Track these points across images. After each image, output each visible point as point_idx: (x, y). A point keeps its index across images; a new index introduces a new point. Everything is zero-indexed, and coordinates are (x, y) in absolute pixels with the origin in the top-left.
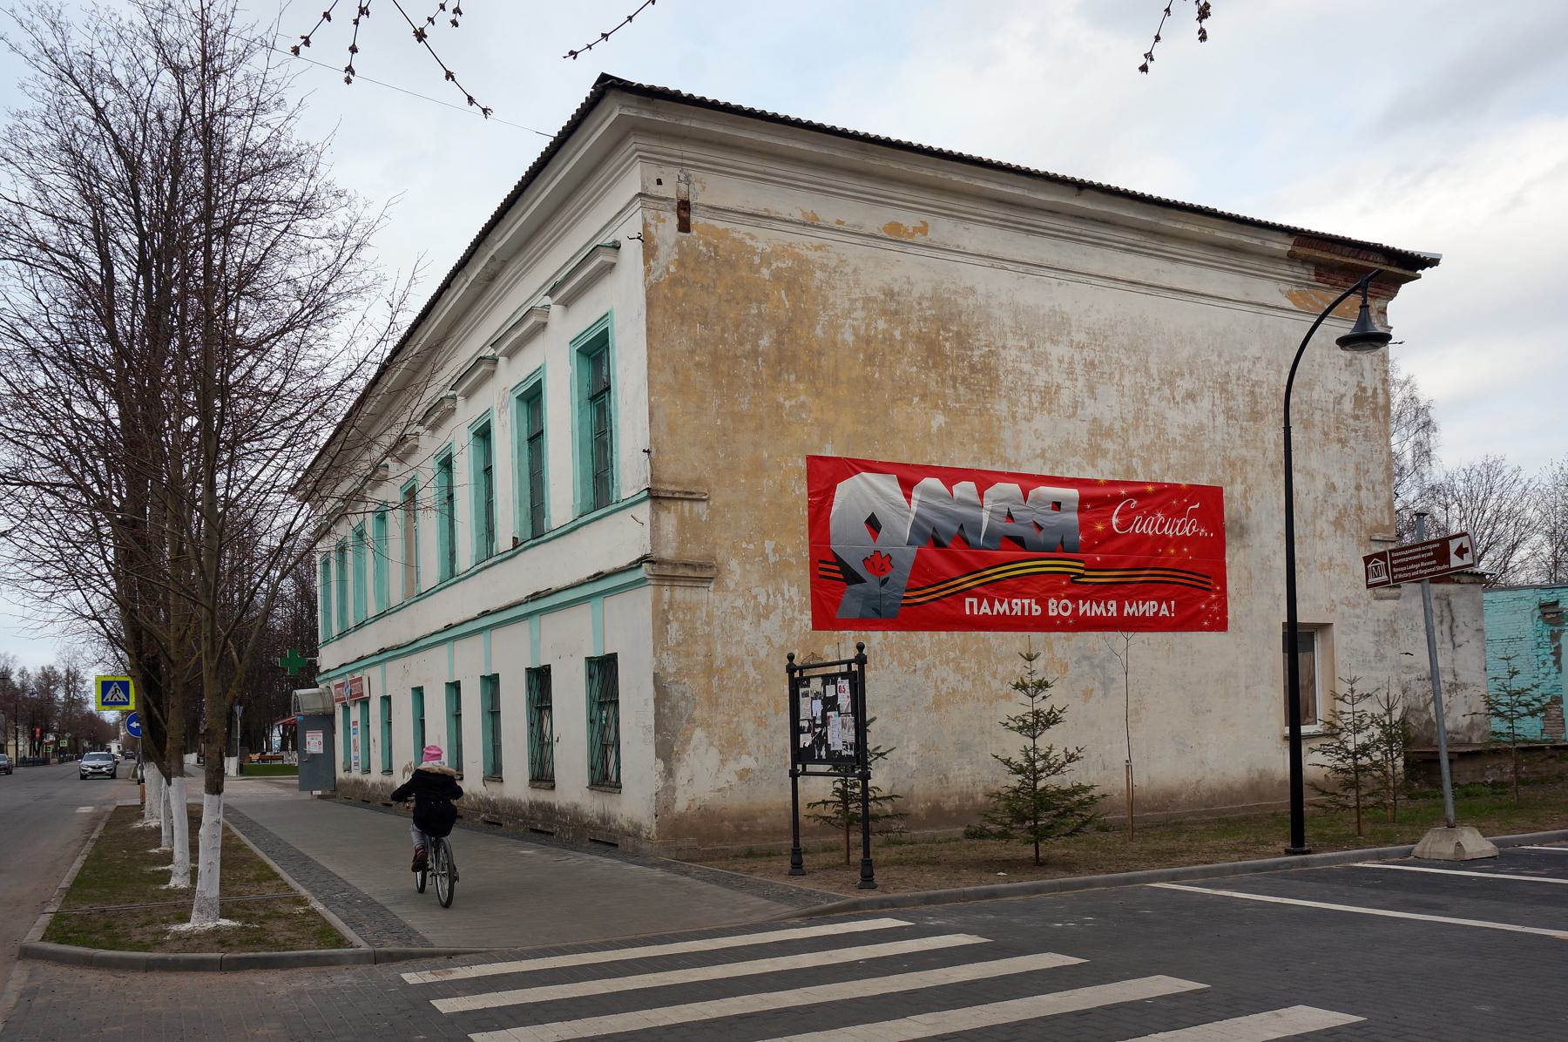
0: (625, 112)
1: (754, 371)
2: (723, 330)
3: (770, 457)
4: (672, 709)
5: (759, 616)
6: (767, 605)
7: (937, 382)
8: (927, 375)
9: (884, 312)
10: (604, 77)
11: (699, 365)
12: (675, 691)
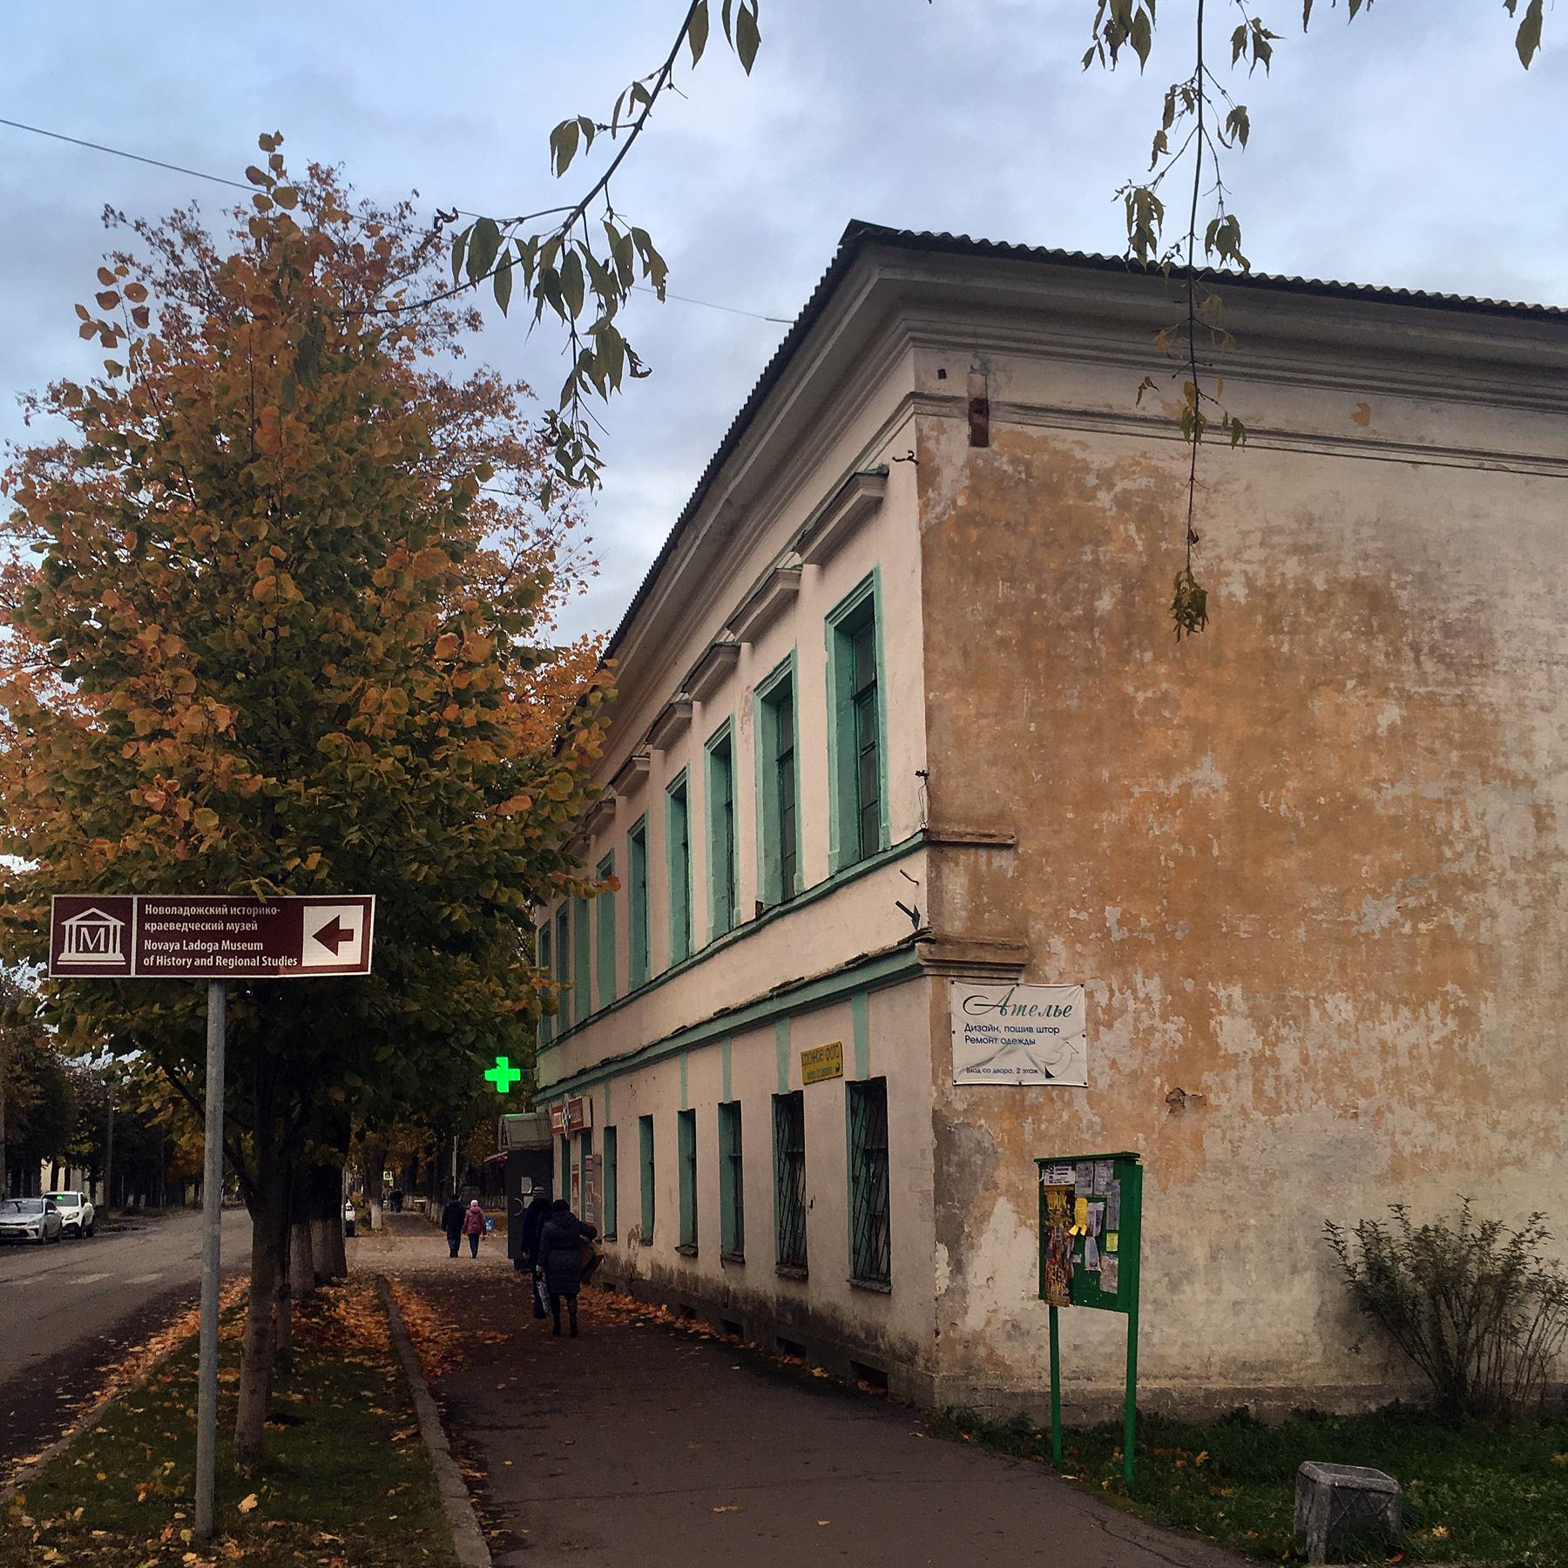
0: (889, 274)
1: (1087, 649)
2: (1039, 590)
3: (1113, 778)
4: (962, 1166)
5: (1097, 1023)
6: (1109, 1006)
7: (1387, 655)
8: (1370, 646)
9: (1296, 549)
10: (855, 226)
11: (1003, 643)
12: (965, 1139)
